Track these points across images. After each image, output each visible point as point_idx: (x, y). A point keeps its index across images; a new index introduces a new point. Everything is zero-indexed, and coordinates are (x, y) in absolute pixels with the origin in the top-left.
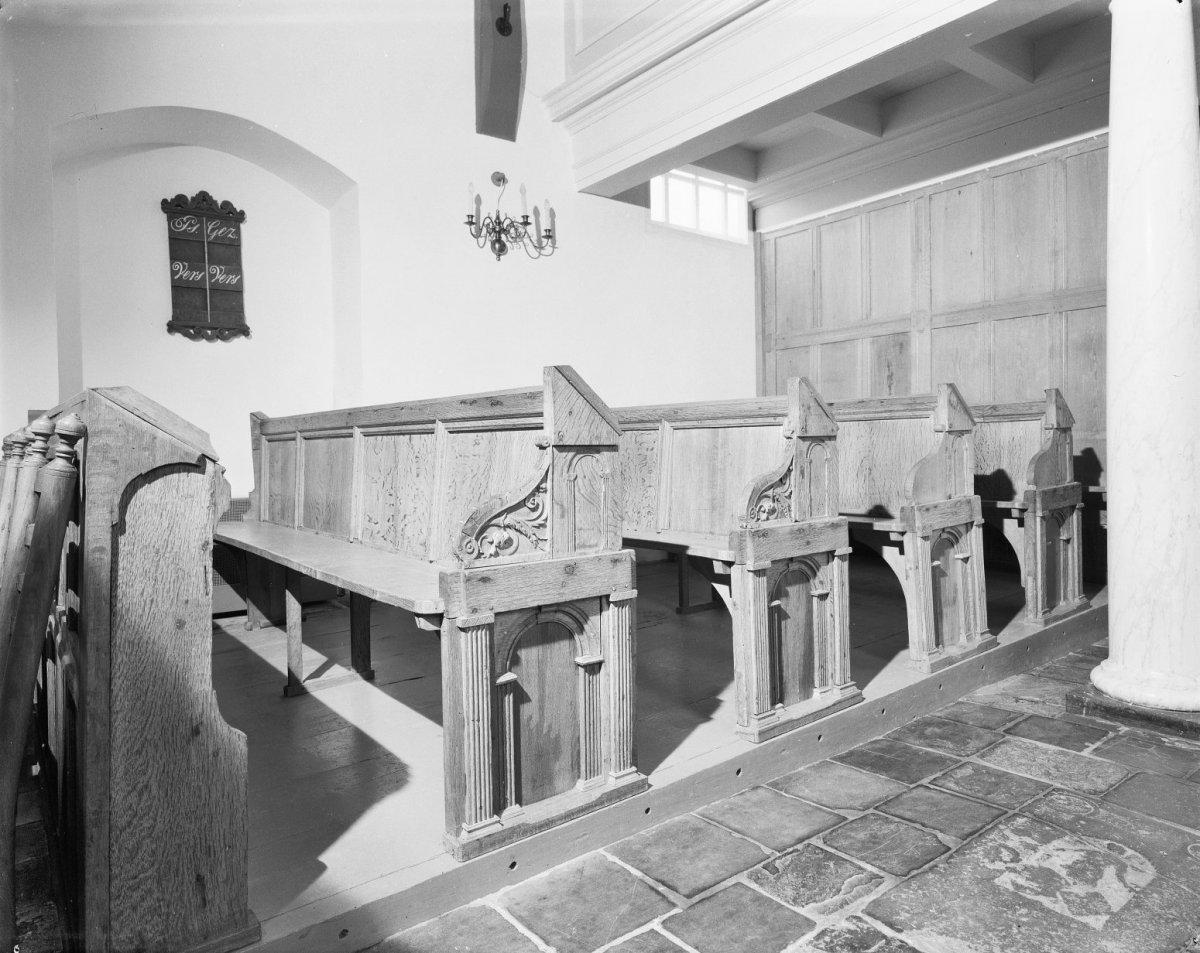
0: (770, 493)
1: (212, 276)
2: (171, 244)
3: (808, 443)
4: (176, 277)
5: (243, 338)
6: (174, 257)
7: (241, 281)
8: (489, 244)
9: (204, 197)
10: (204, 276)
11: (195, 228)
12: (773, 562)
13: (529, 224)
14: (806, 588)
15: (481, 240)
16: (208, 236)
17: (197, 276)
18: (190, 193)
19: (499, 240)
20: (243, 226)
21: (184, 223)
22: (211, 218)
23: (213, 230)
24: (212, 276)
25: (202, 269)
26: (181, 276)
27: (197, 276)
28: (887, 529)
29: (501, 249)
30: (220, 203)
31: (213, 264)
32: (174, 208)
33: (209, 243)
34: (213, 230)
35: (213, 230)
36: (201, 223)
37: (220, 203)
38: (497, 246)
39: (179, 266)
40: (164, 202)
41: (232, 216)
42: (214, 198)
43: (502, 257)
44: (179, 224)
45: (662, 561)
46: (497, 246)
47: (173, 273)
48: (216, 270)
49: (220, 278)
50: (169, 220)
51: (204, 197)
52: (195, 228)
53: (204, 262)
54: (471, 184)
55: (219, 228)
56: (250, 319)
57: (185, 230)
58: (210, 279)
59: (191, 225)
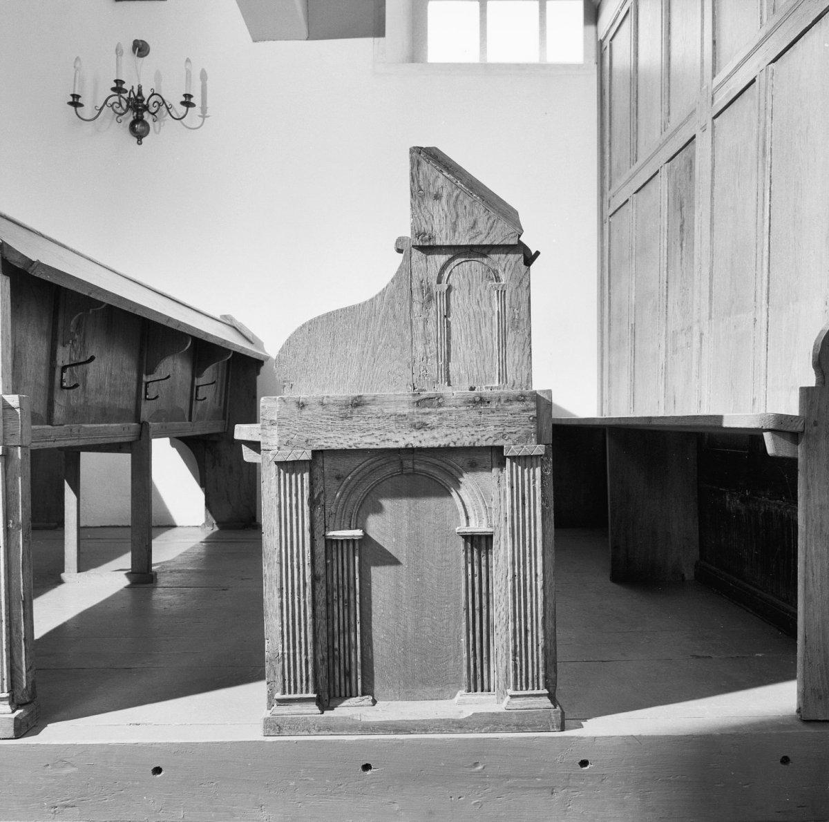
3: (442, 259)
12: (315, 453)
13: (193, 105)
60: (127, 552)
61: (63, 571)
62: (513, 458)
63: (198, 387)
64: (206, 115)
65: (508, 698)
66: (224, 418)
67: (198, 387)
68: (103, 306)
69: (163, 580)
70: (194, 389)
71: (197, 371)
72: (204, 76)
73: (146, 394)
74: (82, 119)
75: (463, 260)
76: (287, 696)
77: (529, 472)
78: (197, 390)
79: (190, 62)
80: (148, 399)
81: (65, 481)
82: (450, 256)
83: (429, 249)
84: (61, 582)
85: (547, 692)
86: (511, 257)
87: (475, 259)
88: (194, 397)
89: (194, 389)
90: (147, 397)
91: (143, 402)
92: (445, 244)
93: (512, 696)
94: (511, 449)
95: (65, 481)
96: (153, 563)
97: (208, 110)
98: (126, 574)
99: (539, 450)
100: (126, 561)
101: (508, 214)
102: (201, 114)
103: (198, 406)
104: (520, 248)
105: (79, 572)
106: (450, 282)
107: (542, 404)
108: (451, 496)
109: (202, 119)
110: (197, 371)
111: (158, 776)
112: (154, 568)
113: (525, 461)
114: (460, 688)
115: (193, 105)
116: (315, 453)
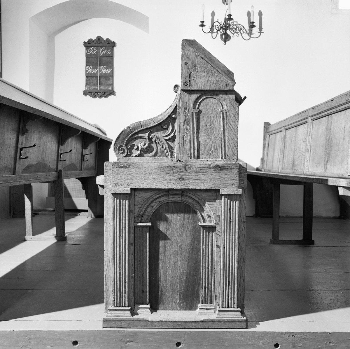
0: (146, 135)
1: (101, 71)
2: (86, 60)
3: (194, 97)
4: (87, 73)
5: (112, 96)
6: (88, 64)
7: (112, 72)
8: (219, 36)
9: (99, 38)
10: (98, 71)
11: (95, 52)
12: (132, 189)
13: (254, 26)
14: (193, 219)
15: (214, 35)
16: (100, 54)
17: (95, 71)
18: (94, 38)
19: (225, 33)
20: (115, 48)
21: (91, 50)
22: (101, 47)
23: (102, 52)
24: (101, 71)
25: (96, 68)
26: (89, 72)
27: (95, 71)
28: (337, 185)
29: (226, 38)
30: (105, 39)
31: (102, 65)
32: (88, 44)
33: (100, 57)
34: (101, 52)
35: (101, 52)
36: (97, 49)
37: (105, 39)
38: (223, 36)
39: (88, 68)
40: (84, 42)
41: (111, 45)
42: (103, 38)
43: (227, 42)
44: (89, 51)
45: (335, 218)
46: (223, 36)
47: (86, 71)
48: (102, 68)
49: (104, 71)
50: (86, 49)
51: (99, 38)
52: (95, 52)
53: (98, 65)
54: (203, 5)
55: (104, 50)
56: (117, 88)
57: (92, 53)
58: (100, 72)
59: (94, 51)
60: (49, 228)
61: (26, 235)
62: (226, 195)
63: (84, 155)
64: (214, 32)
65: (217, 311)
66: (95, 170)
67: (84, 155)
68: (41, 118)
69: (69, 242)
70: (83, 156)
71: (84, 147)
72: (260, 14)
73: (20, 155)
74: (243, 38)
75: (204, 97)
76: (224, 309)
77: (235, 203)
78: (84, 156)
79: (253, 7)
80: (61, 161)
81: (25, 195)
82: (199, 95)
83: (190, 92)
84: (25, 240)
85: (240, 310)
86: (230, 96)
87: (213, 97)
88: (18, 157)
89: (83, 156)
90: (61, 159)
91: (59, 162)
92: (210, 89)
93: (219, 311)
94: (223, 191)
95: (25, 195)
96: (65, 232)
97: (263, 30)
98: (55, 237)
99: (240, 192)
100: (53, 231)
101: (229, 74)
102: (259, 31)
103: (85, 164)
104: (233, 92)
105: (33, 235)
106: (200, 108)
107: (241, 169)
108: (197, 213)
109: (259, 34)
110: (84, 147)
111: (278, 348)
112: (66, 235)
113: (229, 196)
114: (200, 303)
115: (254, 26)
116: (132, 189)
